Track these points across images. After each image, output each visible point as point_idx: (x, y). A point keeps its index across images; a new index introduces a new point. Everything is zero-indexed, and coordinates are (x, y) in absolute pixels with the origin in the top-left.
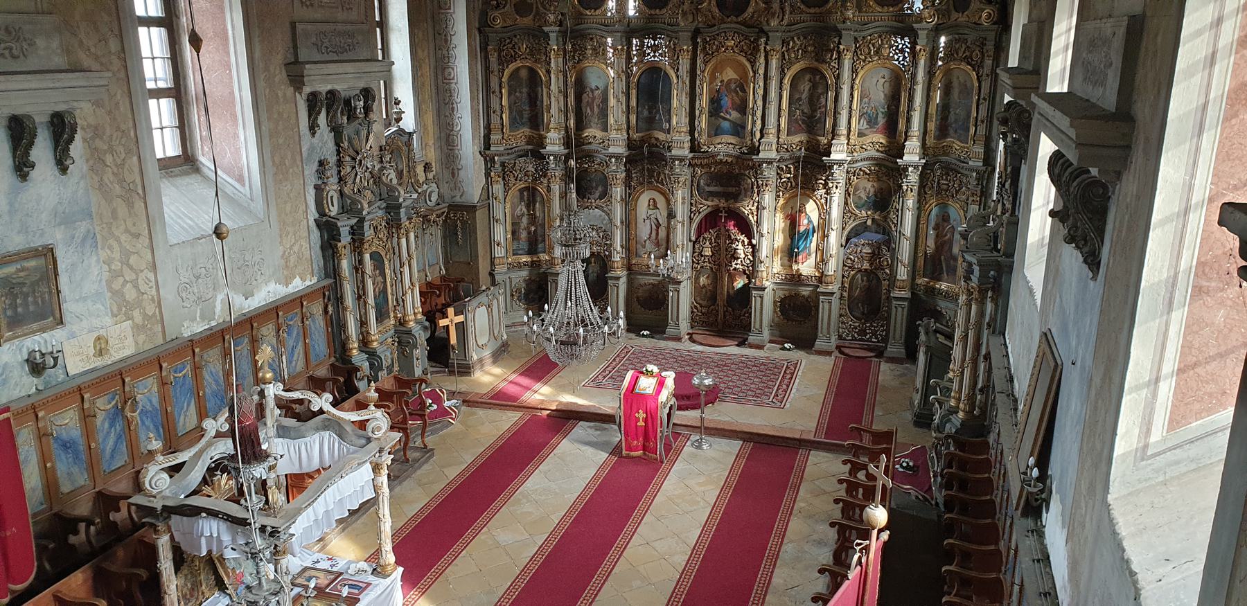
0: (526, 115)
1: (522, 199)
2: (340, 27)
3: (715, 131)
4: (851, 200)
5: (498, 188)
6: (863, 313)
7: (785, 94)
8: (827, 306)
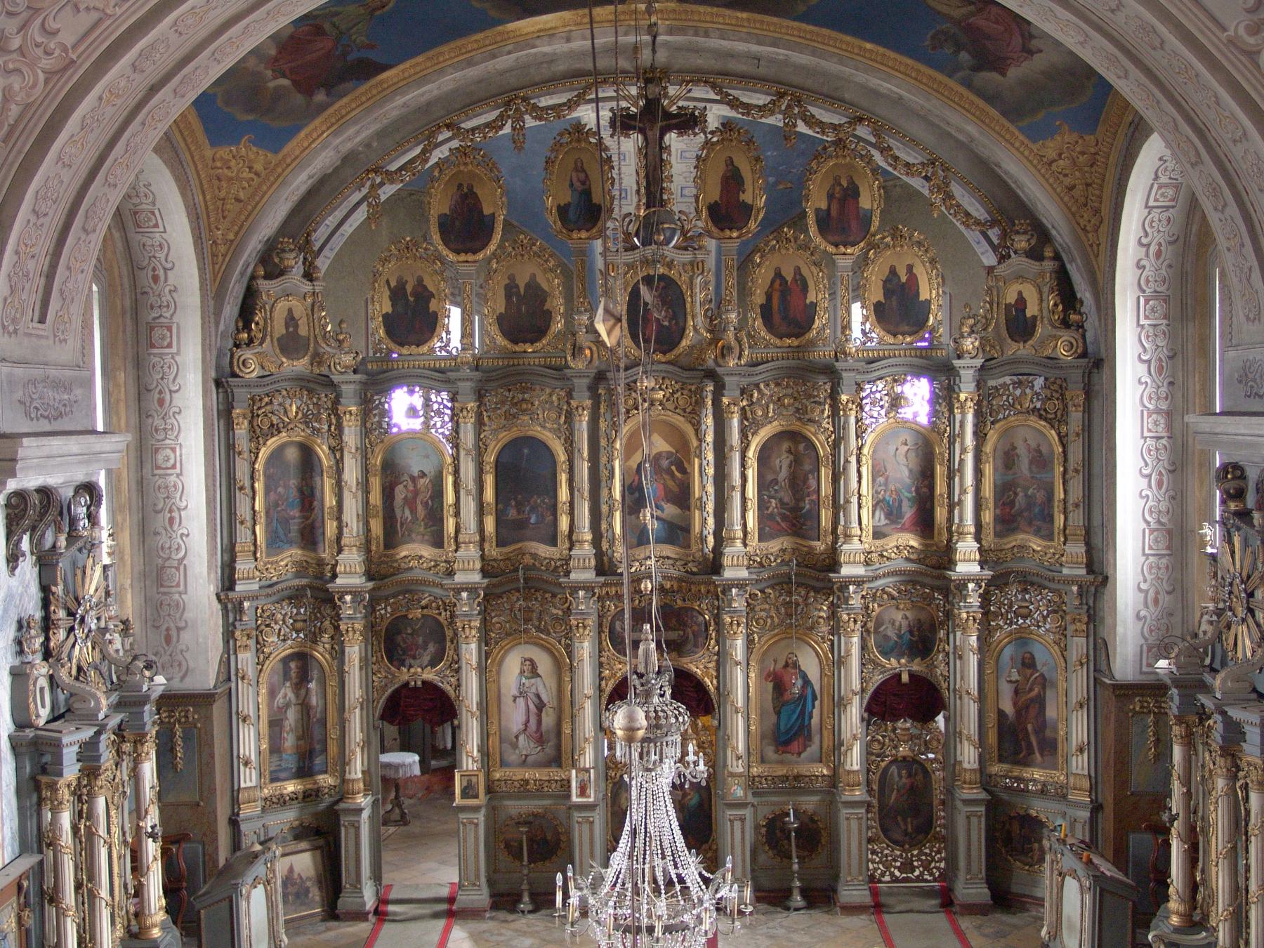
0: (294, 527)
1: (286, 676)
2: (53, 373)
3: (638, 537)
4: (872, 642)
5: (246, 659)
6: (906, 833)
7: (752, 474)
8: (586, 827)
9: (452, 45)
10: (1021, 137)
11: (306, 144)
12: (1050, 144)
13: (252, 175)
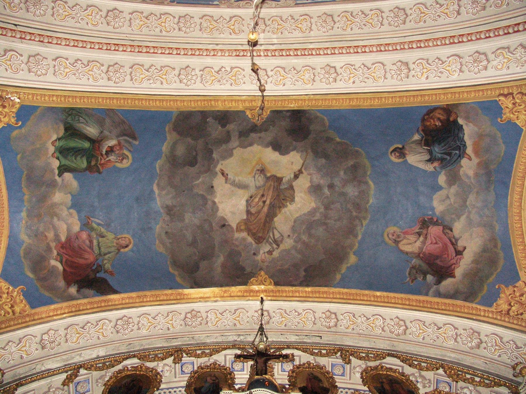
9: (153, 292)
10: (482, 308)
11: (51, 314)
12: (500, 302)
13: (10, 311)
